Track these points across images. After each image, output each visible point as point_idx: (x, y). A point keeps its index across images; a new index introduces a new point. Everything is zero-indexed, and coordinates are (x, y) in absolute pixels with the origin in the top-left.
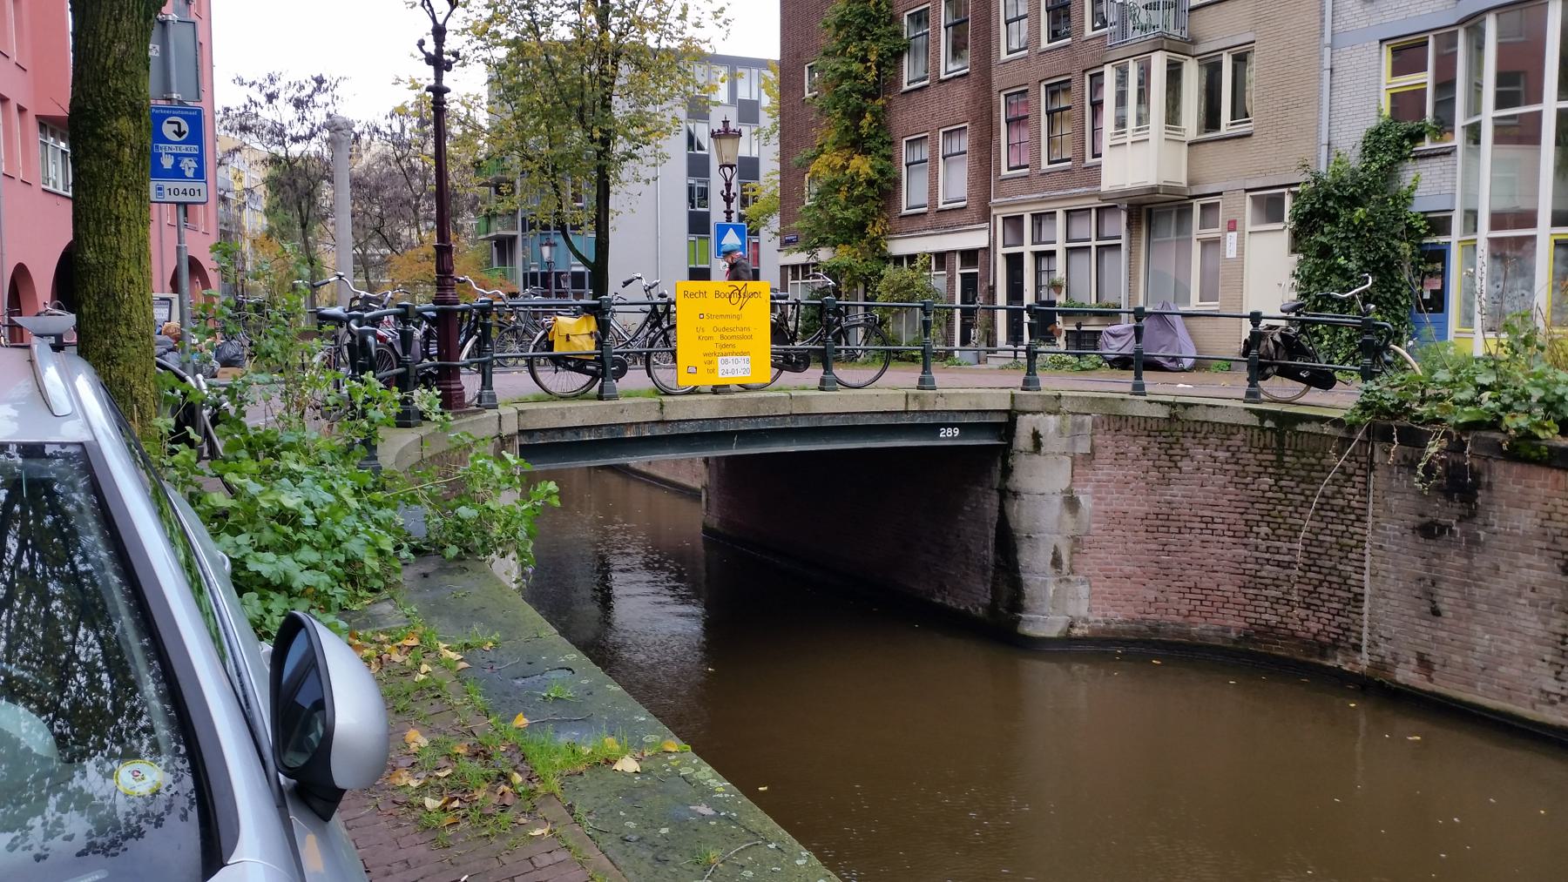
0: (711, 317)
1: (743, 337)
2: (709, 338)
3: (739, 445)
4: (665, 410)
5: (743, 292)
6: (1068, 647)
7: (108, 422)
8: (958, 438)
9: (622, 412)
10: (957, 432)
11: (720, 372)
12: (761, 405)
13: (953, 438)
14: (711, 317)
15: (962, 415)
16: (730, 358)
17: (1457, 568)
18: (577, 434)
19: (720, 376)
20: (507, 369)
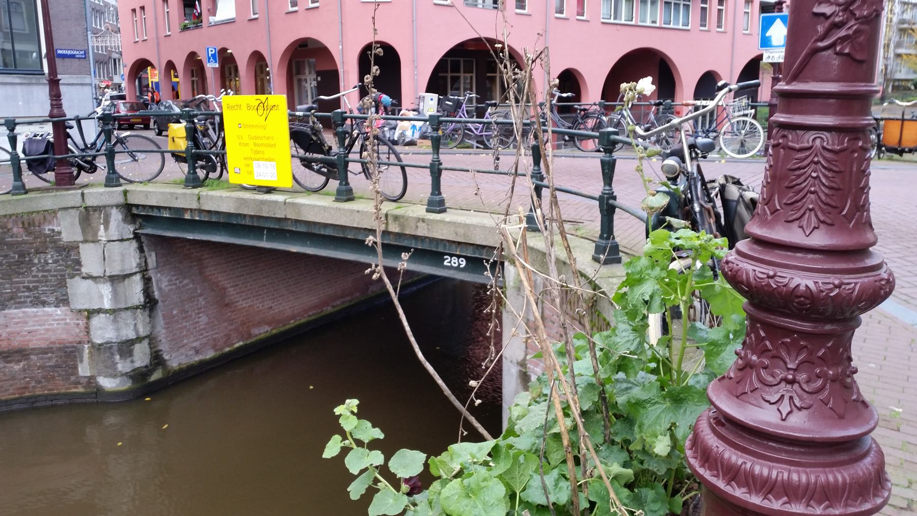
0: (246, 126)
1: (269, 146)
2: (246, 144)
3: (268, 240)
4: (201, 201)
5: (265, 105)
6: (135, 273)
7: (833, 438)
8: (464, 270)
9: (177, 198)
10: (463, 263)
11: (256, 174)
12: (420, 224)
13: (458, 268)
14: (246, 126)
15: (454, 246)
16: (261, 163)
17: (828, 479)
18: (160, 211)
19: (256, 178)
20: (582, 154)
